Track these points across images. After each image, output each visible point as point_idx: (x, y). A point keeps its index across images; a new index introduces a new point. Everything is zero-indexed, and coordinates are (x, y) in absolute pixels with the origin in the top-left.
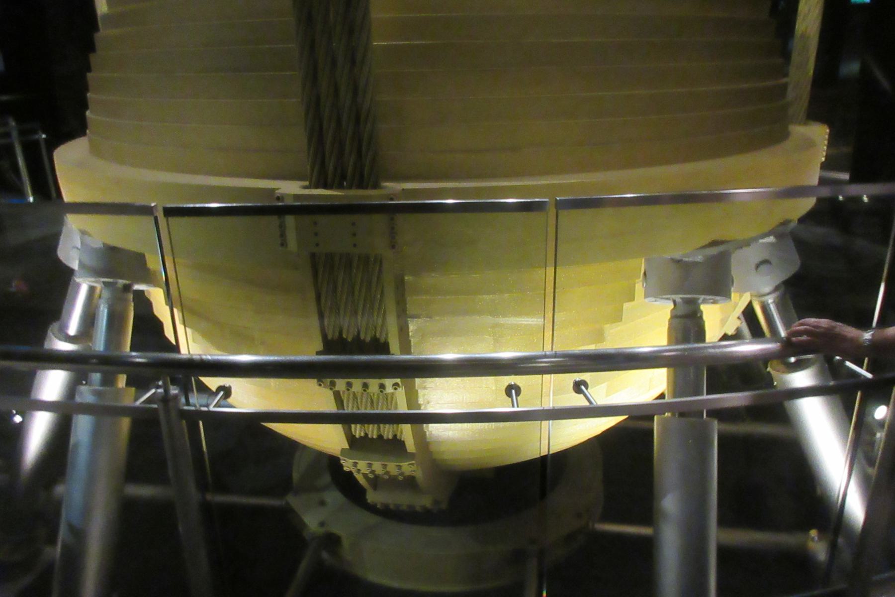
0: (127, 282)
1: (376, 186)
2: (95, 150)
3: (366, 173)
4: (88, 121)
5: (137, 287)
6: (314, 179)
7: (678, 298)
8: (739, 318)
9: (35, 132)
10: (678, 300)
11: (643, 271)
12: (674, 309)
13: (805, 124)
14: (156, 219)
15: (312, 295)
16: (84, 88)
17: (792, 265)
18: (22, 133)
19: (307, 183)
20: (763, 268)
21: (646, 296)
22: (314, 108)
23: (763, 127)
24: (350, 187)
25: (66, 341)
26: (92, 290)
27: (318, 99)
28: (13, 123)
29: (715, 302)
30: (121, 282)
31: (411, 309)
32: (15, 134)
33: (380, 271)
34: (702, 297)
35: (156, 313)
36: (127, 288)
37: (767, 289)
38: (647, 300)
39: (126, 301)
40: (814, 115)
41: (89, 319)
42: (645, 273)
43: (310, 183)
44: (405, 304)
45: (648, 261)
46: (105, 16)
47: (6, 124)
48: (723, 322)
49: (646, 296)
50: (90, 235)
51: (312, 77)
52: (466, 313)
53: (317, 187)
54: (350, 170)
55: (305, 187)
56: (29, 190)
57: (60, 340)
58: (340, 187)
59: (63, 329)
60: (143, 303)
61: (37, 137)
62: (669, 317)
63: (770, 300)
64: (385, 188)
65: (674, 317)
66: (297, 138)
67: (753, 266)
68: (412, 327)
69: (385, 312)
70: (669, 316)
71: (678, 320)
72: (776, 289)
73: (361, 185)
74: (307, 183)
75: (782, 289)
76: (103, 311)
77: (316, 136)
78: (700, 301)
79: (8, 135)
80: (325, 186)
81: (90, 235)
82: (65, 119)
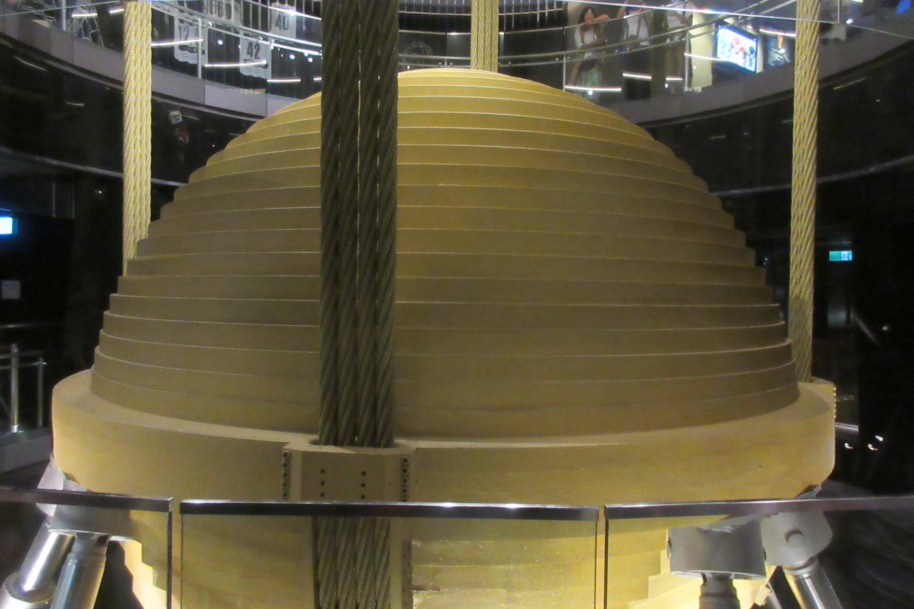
0: (104, 534)
1: (389, 444)
2: (97, 388)
3: (380, 429)
4: (96, 358)
5: (114, 538)
6: (325, 434)
7: (708, 573)
8: (767, 586)
9: (35, 359)
10: (708, 573)
11: (667, 540)
12: (704, 585)
13: (811, 381)
14: (170, 514)
15: (309, 562)
16: (98, 322)
17: (825, 537)
18: (22, 360)
19: (316, 437)
20: (793, 538)
21: (673, 569)
22: (332, 361)
23: (772, 389)
24: (361, 445)
25: (19, 598)
26: (61, 539)
27: (337, 353)
28: (15, 349)
29: (745, 578)
30: (98, 534)
31: (417, 580)
32: (14, 361)
33: (387, 536)
34: (734, 573)
35: (54, 390)
36: (102, 540)
37: (801, 563)
38: (673, 573)
39: (99, 555)
40: (819, 371)
41: (53, 573)
42: (669, 542)
43: (321, 437)
44: (411, 573)
45: (673, 532)
46: (131, 263)
47: (8, 351)
48: (754, 593)
49: (673, 569)
50: (74, 480)
51: (333, 332)
52: (478, 585)
53: (327, 444)
54: (363, 426)
55: (314, 443)
56: (15, 417)
57: (14, 596)
58: (352, 444)
59: (19, 583)
60: (116, 552)
61: (37, 363)
62: (699, 594)
63: (805, 574)
64: (396, 445)
65: (704, 595)
66: (313, 390)
67: (783, 537)
68: (416, 600)
69: (389, 583)
70: (698, 593)
71: (711, 599)
72: (810, 561)
73: (374, 444)
74: (316, 437)
75: (816, 564)
76: (71, 566)
77: (332, 390)
78: (732, 577)
79: (7, 362)
80: (336, 443)
81: (74, 480)
82: (72, 356)
